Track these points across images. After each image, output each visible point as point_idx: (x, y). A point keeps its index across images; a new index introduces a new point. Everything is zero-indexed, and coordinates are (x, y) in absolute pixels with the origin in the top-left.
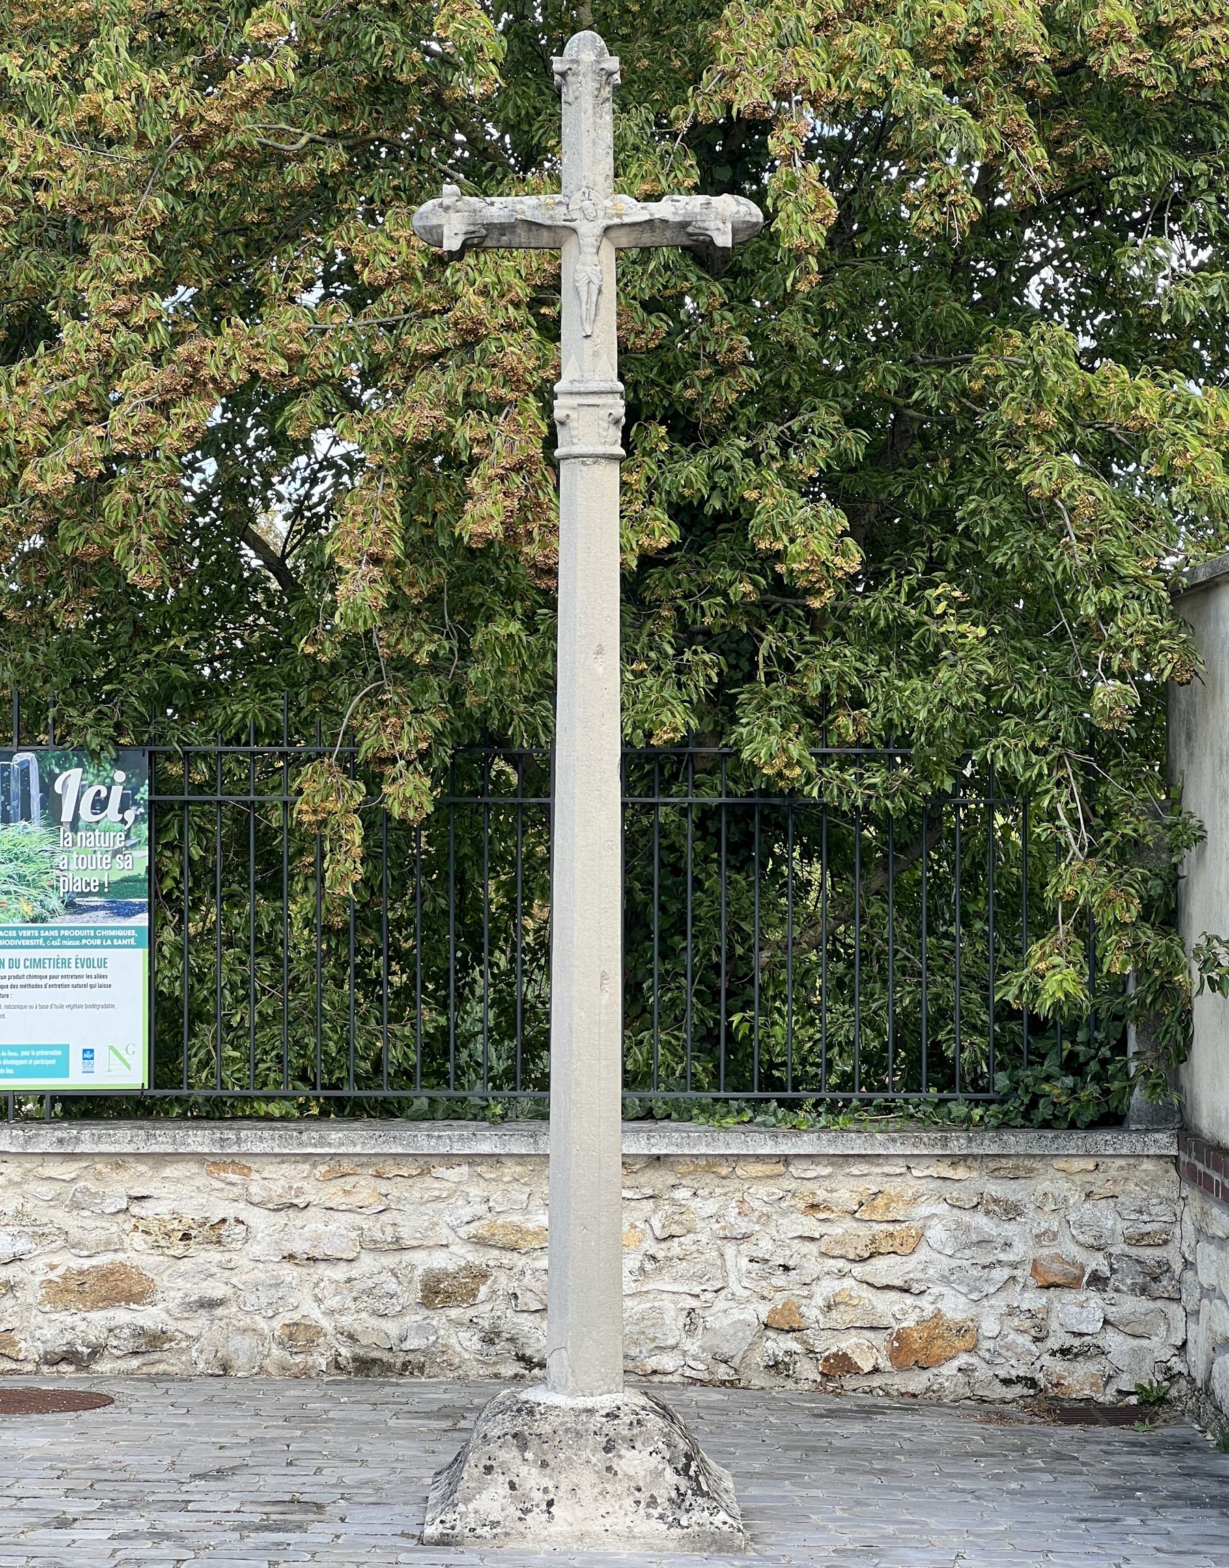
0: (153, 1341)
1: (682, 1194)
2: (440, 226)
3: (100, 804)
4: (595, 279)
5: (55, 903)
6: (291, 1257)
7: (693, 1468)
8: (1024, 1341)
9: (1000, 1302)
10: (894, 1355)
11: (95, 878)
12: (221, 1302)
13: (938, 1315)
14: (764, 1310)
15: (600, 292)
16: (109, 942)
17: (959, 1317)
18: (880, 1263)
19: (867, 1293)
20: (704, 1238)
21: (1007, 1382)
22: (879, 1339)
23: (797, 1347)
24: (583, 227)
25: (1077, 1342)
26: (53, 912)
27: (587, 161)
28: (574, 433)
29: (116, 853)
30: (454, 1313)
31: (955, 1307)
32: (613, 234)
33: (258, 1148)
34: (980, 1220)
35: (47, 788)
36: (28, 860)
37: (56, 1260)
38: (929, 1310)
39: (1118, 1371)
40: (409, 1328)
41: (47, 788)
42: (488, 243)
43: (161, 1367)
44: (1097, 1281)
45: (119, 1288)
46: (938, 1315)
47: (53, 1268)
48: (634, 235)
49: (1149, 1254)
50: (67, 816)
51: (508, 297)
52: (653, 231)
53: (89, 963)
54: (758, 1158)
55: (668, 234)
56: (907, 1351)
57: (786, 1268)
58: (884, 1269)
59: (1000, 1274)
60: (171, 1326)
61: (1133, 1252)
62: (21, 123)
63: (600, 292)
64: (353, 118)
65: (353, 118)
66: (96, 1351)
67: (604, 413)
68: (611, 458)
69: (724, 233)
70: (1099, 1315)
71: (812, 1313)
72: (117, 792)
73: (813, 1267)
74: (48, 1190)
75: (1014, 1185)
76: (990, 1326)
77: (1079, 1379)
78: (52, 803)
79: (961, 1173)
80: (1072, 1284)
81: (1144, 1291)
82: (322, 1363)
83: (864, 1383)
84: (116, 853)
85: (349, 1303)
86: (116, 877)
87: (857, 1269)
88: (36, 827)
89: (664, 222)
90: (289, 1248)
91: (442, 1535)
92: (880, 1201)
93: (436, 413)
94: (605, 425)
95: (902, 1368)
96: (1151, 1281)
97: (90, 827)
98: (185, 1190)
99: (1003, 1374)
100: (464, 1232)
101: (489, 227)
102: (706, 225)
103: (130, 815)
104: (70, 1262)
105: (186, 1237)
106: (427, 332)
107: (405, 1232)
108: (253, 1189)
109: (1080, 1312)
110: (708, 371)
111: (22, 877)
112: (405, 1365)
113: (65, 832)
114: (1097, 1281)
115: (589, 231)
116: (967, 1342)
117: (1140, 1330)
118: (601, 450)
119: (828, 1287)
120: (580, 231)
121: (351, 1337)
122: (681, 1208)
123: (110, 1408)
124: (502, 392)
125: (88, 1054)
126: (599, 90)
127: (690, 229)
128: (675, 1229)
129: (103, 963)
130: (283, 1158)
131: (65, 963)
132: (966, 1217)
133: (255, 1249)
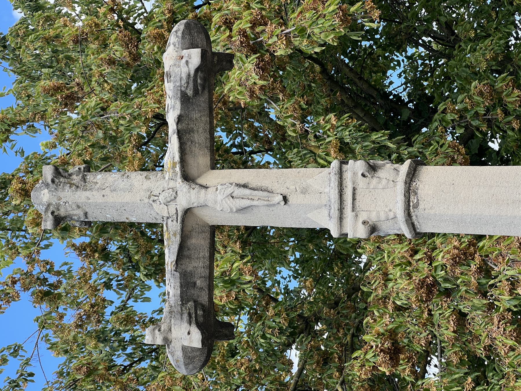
2: (184, 349)
4: (229, 191)
15: (245, 186)
24: (182, 203)
27: (127, 198)
28: (383, 217)
32: (193, 171)
42: (204, 299)
48: (196, 150)
51: (410, 259)
52: (192, 131)
55: (195, 115)
63: (245, 186)
64: (332, 353)
65: (332, 353)
67: (362, 182)
68: (412, 175)
69: (189, 56)
93: (496, 321)
94: (375, 181)
101: (184, 298)
102: (184, 76)
106: (443, 322)
110: (499, 111)
115: (187, 196)
118: (400, 187)
120: (186, 206)
124: (473, 268)
126: (71, 185)
127: (190, 93)
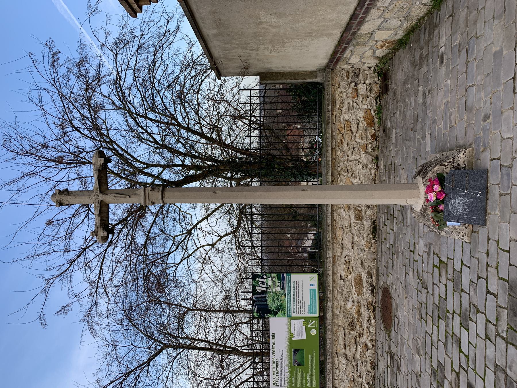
0: (369, 274)
1: (339, 169)
3: (263, 283)
5: (282, 292)
6: (352, 247)
7: (445, 164)
8: (368, 100)
9: (360, 105)
10: (371, 126)
11: (277, 284)
12: (362, 261)
13: (363, 117)
14: (362, 152)
16: (290, 281)
17: (363, 113)
18: (353, 129)
19: (359, 132)
20: (348, 165)
21: (376, 103)
22: (368, 129)
23: (370, 146)
25: (368, 89)
26: (284, 292)
29: (272, 280)
30: (363, 214)
31: (361, 114)
33: (331, 254)
34: (344, 109)
35: (260, 293)
36: (274, 297)
37: (353, 293)
38: (362, 119)
39: (374, 81)
40: (367, 223)
41: (260, 293)
43: (375, 273)
44: (356, 85)
45: (359, 281)
46: (363, 117)
47: (355, 294)
49: (351, 74)
50: (265, 289)
53: (294, 285)
54: (332, 154)
56: (371, 123)
57: (354, 148)
58: (354, 128)
59: (355, 105)
60: (367, 271)
61: (350, 78)
62: (416, 46)
66: (371, 285)
67: (150, 193)
70: (363, 85)
71: (363, 142)
72: (260, 280)
73: (354, 143)
74: (339, 295)
75: (337, 102)
76: (365, 107)
77: (376, 89)
78: (263, 292)
79: (335, 113)
80: (357, 90)
81: (358, 76)
82: (374, 241)
83: (377, 132)
84: (272, 280)
85: (361, 235)
86: (277, 280)
87: (354, 134)
88: (268, 295)
89: (98, 177)
90: (350, 247)
91: (468, 236)
92: (340, 129)
95: (374, 124)
96: (356, 75)
97: (267, 285)
98: (339, 268)
99: (375, 104)
100: (347, 213)
103: (265, 277)
104: (353, 290)
105: (349, 268)
107: (347, 224)
108: (339, 254)
109: (362, 89)
111: (277, 298)
112: (373, 224)
113: (269, 290)
114: (356, 85)
116: (369, 111)
117: (366, 76)
119: (358, 140)
121: (368, 235)
122: (342, 169)
123: (392, 291)
125: (311, 285)
128: (346, 170)
129: (294, 282)
130: (333, 249)
131: (294, 290)
132: (343, 112)
133: (351, 254)
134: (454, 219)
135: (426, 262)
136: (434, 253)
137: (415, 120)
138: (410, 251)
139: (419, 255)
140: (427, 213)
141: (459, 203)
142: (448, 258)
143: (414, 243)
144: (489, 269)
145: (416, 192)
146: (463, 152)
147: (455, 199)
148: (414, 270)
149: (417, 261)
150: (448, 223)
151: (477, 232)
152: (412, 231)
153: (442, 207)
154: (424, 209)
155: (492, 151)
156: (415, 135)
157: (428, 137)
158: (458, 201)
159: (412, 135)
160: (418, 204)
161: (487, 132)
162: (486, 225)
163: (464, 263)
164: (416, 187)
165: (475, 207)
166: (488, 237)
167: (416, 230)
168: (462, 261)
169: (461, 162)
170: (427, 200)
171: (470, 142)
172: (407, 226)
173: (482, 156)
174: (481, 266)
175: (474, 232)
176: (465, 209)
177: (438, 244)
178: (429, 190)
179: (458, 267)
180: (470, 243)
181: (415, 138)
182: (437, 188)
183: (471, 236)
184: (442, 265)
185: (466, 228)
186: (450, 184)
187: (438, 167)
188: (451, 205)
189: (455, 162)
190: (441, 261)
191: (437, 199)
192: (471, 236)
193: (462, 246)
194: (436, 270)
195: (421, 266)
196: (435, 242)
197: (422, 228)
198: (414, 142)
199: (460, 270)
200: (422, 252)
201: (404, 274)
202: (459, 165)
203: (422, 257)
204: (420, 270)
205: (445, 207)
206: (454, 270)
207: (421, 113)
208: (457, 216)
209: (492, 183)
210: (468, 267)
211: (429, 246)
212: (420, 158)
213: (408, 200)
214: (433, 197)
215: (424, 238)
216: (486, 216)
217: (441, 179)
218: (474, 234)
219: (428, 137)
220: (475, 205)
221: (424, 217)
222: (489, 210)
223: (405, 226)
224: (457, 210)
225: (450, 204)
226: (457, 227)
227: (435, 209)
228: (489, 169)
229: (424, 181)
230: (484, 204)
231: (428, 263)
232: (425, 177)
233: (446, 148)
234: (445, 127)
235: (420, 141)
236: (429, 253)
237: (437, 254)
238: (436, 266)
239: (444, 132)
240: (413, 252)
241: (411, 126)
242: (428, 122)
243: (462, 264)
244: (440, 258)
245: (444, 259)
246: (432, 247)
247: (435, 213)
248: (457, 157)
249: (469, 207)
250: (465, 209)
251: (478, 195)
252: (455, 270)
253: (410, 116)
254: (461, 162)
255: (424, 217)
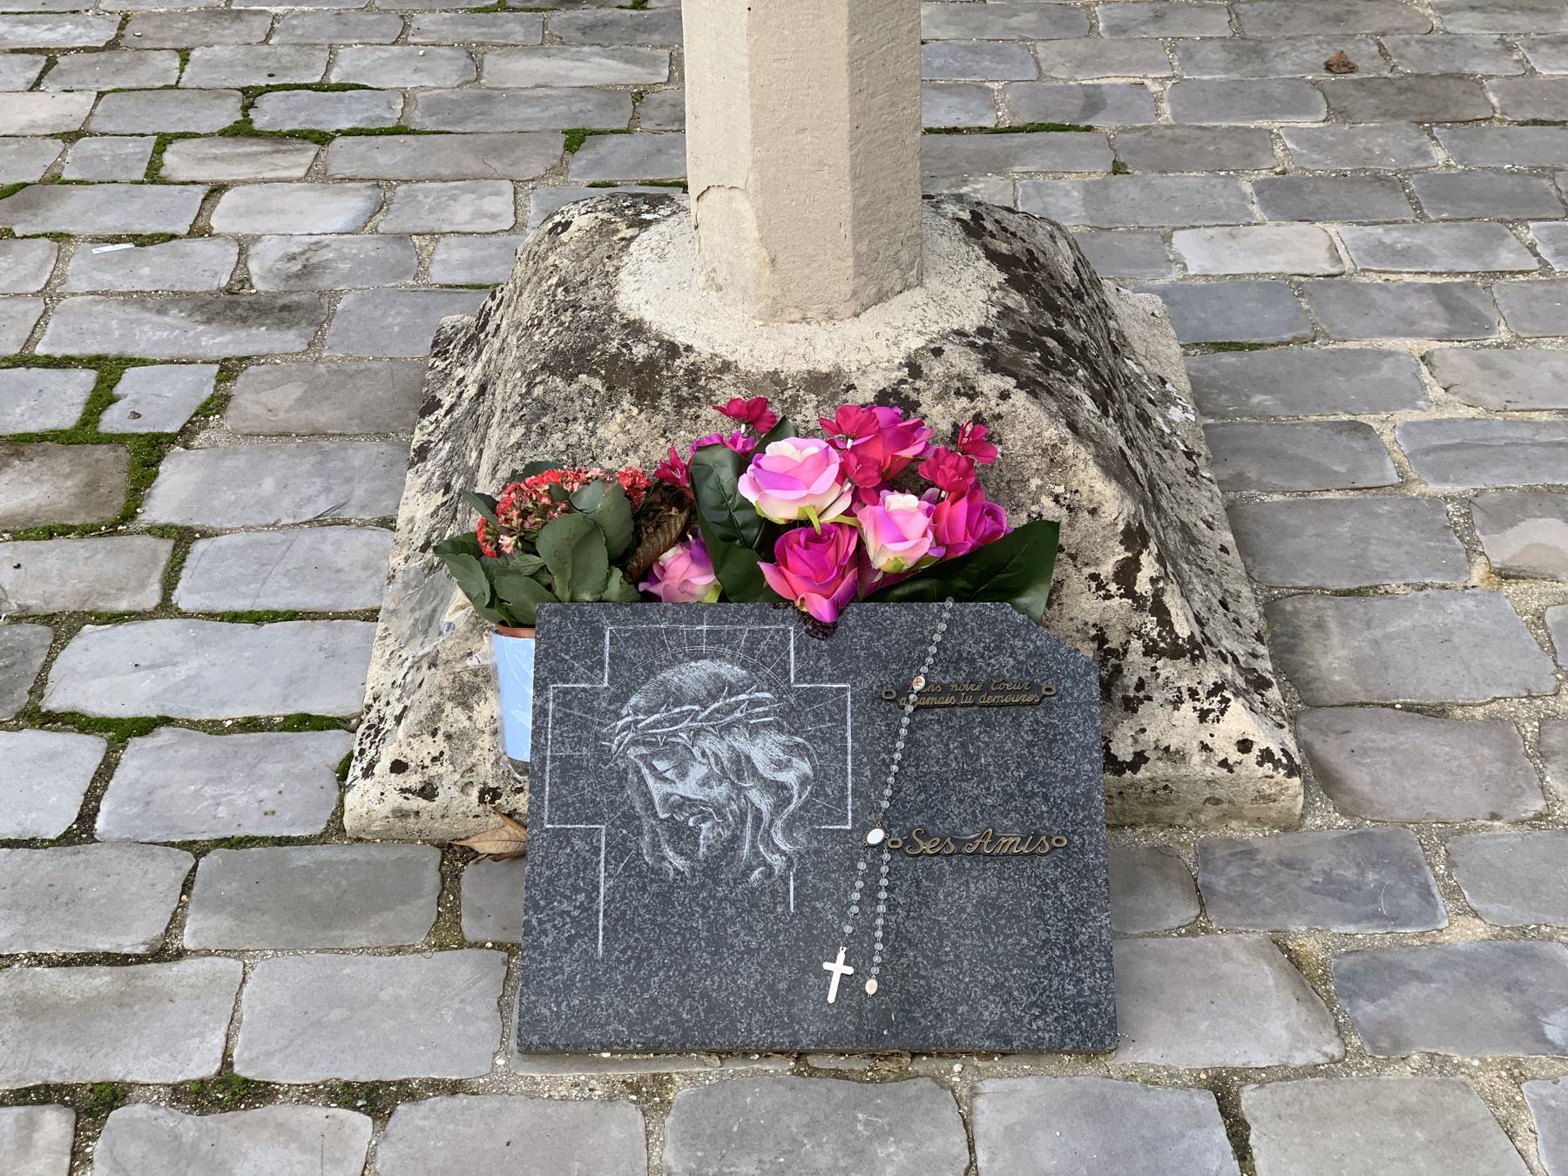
134: (566, 715)
135: (151, 271)
136: (228, 369)
137: (1433, 100)
138: (250, 96)
139: (217, 190)
140: (611, 400)
141: (742, 764)
142: (183, 538)
143: (323, 139)
144: (55, 1124)
145: (837, 272)
146: (1263, 738)
147: (788, 719)
148: (70, 137)
149: (154, 175)
150: (515, 656)
151: (447, 933)
152: (433, 107)
153: (685, 573)
154: (648, 373)
155: (1321, 1094)
156: (1296, 104)
157: (1302, 248)
158: (763, 751)
159: (1285, 68)
160: (700, 290)
161: (1501, 1007)
162: (527, 1051)
163: (136, 758)
164: (883, 273)
165: (717, 942)
166: (406, 1092)
167: (446, 154)
168: (145, 726)
169: (1172, 725)
170: (761, 419)
171: (1358, 777)
172: (474, 55)
173: (1237, 954)
174: (88, 1007)
175: (449, 881)
176: (681, 835)
177: (324, 416)
178: (881, 440)
179: (95, 675)
180: (335, 829)
181: (1268, 105)
182: (902, 532)
183: (406, 839)
184: (113, 465)
185: (489, 795)
186: (951, 659)
187: (1114, 504)
188: (720, 687)
189: (1166, 668)
190: (148, 453)
191: (771, 531)
192: (406, 839)
193: (303, 723)
194: (59, 401)
195: (110, 222)
196: (344, 375)
197: (462, 213)
198: (1229, 95)
199: (54, 701)
200: (243, 228)
201: (42, 35)
202: (1131, 706)
203: (199, 231)
204: (69, 212)
205: (695, 611)
206: (63, 626)
207: (1507, 154)
208: (603, 755)
209: (987, 1116)
210: (87, 816)
211: (297, 304)
212: (1100, 173)
213: (745, 208)
214: (795, 483)
215: (365, 246)
216: (620, 1047)
217: (994, 564)
218: (432, 879)
219: (1302, 248)
220: (738, 936)
221: (567, 363)
222: (690, 1078)
223: (474, 33)
224: (667, 749)
225: (731, 671)
226: (484, 711)
227: (668, 502)
228: (1128, 1058)
229: (962, 361)
230: (750, 1028)
231: (139, 299)
232: (993, 363)
233: (1234, 444)
234: (1449, 449)
235: (1248, 160)
236: (232, 304)
237: (216, 405)
238: (102, 398)
239: (1388, 426)
240: (241, 131)
241: (1364, 54)
242: (1442, 249)
243: (121, 732)
244: (185, 436)
245: (174, 492)
246: (290, 340)
247: (617, 522)
248: (1211, 677)
249: (710, 871)
250: (681, 835)
251: (838, 968)
252: (59, 643)
253: (1451, 40)
254: (1172, 725)
255: (567, 363)
